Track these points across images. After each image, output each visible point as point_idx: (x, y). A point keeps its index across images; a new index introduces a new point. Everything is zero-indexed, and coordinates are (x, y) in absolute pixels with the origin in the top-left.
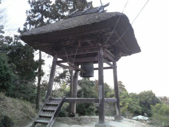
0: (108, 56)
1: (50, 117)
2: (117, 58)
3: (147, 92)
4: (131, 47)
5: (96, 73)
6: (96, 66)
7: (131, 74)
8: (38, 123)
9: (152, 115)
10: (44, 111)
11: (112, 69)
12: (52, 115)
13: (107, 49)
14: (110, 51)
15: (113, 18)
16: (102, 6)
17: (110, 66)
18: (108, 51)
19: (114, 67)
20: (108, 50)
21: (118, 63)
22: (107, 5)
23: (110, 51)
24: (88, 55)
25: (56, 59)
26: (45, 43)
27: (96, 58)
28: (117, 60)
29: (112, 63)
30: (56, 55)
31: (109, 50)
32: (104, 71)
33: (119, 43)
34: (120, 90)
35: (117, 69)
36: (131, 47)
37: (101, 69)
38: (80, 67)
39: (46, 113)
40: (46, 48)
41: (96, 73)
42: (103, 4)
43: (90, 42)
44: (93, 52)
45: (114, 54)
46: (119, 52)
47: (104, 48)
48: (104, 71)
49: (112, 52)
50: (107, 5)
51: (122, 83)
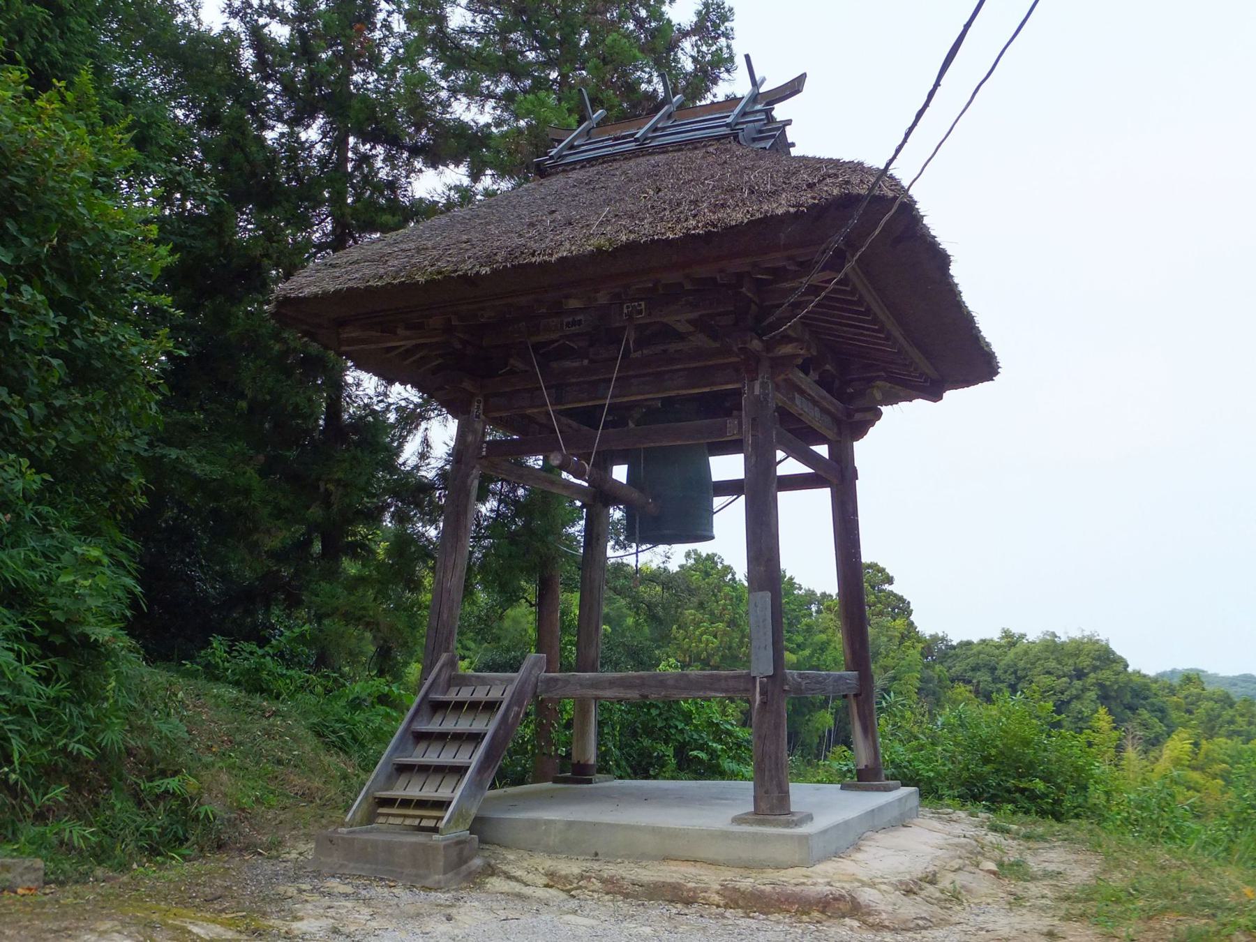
0: (800, 406)
1: (460, 771)
2: (858, 416)
3: (1063, 643)
4: (949, 353)
5: (730, 518)
6: (728, 467)
7: (953, 520)
8: (389, 802)
9: (724, 18)
10: (421, 737)
11: (828, 490)
12: (471, 758)
13: (796, 370)
14: (814, 375)
15: (848, 202)
16: (755, 97)
17: (808, 470)
18: (799, 377)
19: (839, 479)
20: (802, 375)
21: (866, 452)
22: (794, 87)
23: (814, 375)
24: (670, 410)
25: (475, 432)
26: (408, 333)
27: (731, 424)
28: (860, 430)
29: (822, 450)
30: (476, 408)
31: (807, 374)
32: (787, 501)
33: (868, 329)
34: (878, 631)
35: (863, 487)
36: (949, 353)
37: (760, 494)
38: (620, 473)
39: (422, 746)
40: (407, 362)
41: (730, 518)
42: (763, 80)
43: (689, 322)
44: (707, 390)
45: (839, 395)
46: (870, 380)
47: (780, 364)
48: (787, 501)
49: (823, 383)
50: (794, 87)
51: (890, 580)
